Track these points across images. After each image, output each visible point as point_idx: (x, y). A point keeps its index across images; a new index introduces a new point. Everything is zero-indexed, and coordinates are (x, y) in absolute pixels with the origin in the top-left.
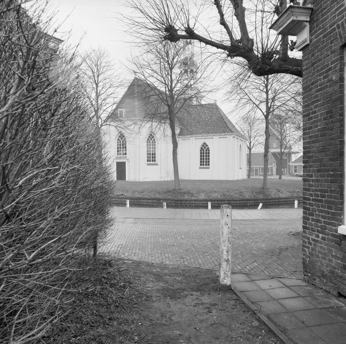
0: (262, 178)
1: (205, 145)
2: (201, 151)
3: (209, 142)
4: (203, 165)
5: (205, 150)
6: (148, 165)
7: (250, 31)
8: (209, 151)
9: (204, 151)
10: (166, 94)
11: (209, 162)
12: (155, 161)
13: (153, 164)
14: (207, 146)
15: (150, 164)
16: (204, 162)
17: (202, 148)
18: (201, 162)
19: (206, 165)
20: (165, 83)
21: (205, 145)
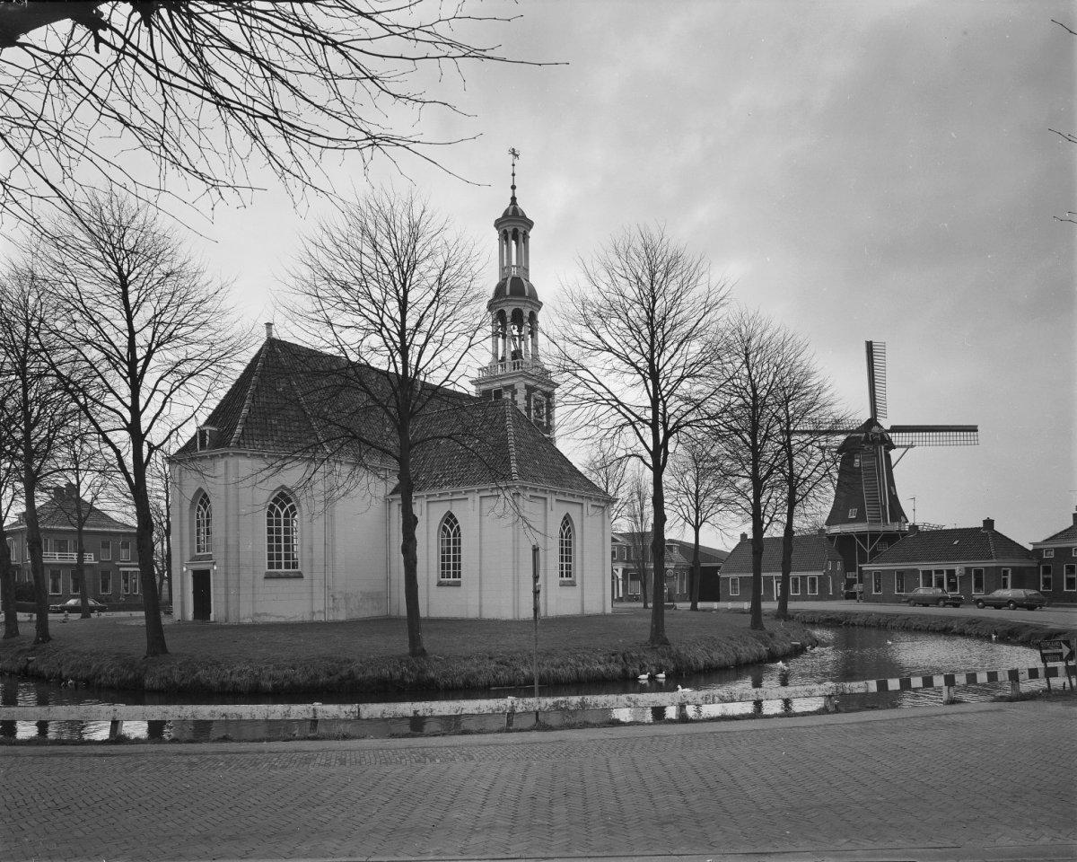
3: (458, 511)
4: (279, 566)
5: (282, 514)
9: (278, 515)
12: (295, 566)
15: (279, 577)
16: (279, 557)
17: (272, 507)
18: (270, 557)
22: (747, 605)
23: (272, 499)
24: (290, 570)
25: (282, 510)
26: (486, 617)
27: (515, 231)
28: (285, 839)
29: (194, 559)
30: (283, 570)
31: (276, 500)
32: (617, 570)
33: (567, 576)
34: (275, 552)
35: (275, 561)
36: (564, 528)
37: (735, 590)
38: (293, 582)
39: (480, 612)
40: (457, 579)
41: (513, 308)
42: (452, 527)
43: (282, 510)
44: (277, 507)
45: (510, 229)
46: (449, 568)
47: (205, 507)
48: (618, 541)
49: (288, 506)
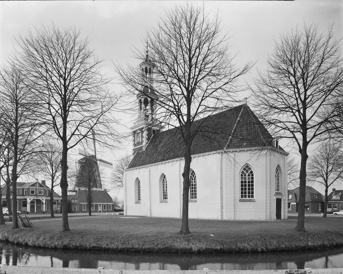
0: (17, 187)
1: (247, 168)
2: (242, 175)
4: (245, 196)
5: (247, 175)
6: (167, 199)
7: (70, 176)
8: (253, 175)
9: (245, 175)
10: (51, 193)
11: (253, 193)
12: (253, 197)
13: (250, 201)
14: (250, 169)
15: (244, 201)
17: (243, 172)
18: (242, 193)
19: (249, 197)
20: (214, 111)
21: (247, 168)
22: (297, 215)
23: (243, 169)
24: (243, 198)
25: (247, 173)
26: (47, 257)
28: (71, 91)
29: (277, 193)
30: (247, 198)
31: (244, 169)
32: (43, 200)
33: (248, 197)
34: (251, 187)
35: (244, 191)
36: (276, 172)
37: (84, 209)
38: (249, 203)
39: (151, 213)
40: (166, 200)
42: (193, 176)
43: (247, 173)
44: (245, 172)
46: (193, 195)
47: (193, 176)
48: (44, 187)
49: (249, 171)
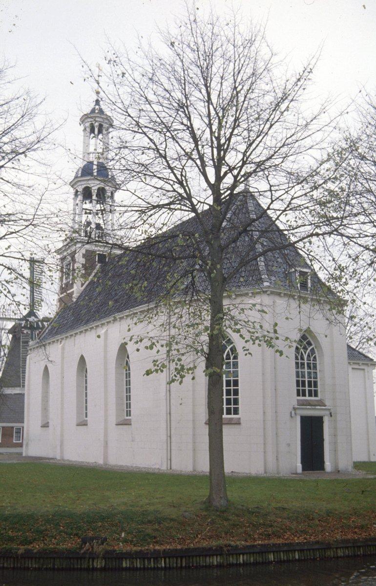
4: (304, 395)
5: (305, 357)
11: (236, 402)
12: (236, 411)
14: (309, 344)
27: (101, 126)
41: (83, 187)
45: (88, 124)
